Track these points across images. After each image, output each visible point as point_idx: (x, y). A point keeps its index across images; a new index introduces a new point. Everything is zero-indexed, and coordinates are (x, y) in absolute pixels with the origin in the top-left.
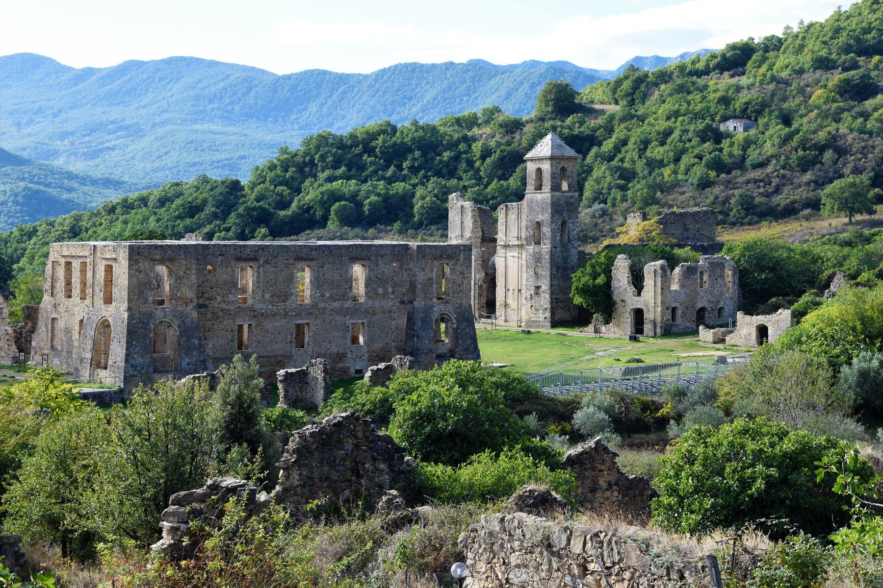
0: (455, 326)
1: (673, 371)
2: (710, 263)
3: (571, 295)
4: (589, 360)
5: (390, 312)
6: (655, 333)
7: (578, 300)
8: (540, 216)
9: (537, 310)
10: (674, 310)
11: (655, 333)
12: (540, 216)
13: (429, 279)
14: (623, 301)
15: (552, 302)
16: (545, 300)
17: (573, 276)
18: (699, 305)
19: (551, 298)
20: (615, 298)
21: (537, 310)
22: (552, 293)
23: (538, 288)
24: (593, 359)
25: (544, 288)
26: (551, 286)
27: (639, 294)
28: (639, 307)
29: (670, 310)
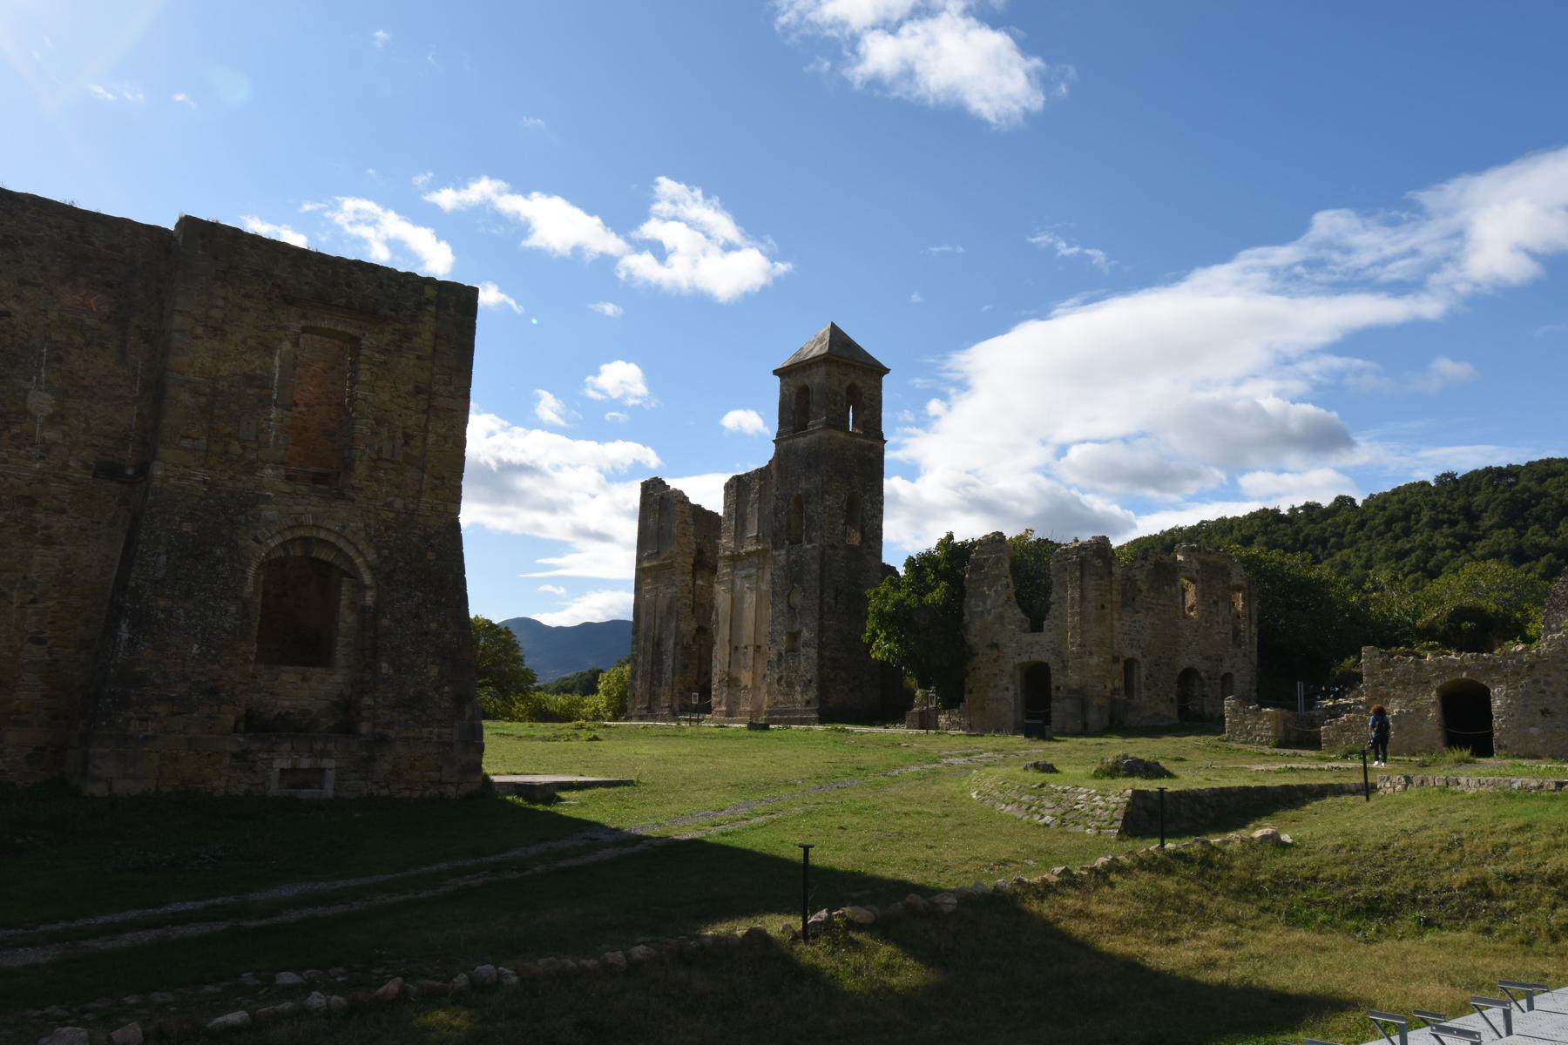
0: (369, 598)
1: (1425, 833)
2: (1201, 562)
3: (866, 637)
4: (922, 777)
5: (31, 501)
6: (1085, 725)
7: (882, 649)
8: (803, 484)
9: (790, 685)
10: (1129, 665)
11: (1085, 725)
12: (803, 484)
13: (250, 379)
14: (994, 646)
15: (821, 666)
16: (807, 663)
17: (870, 593)
18: (1184, 662)
19: (820, 656)
20: (973, 638)
21: (790, 685)
22: (821, 647)
23: (794, 636)
24: (935, 773)
25: (806, 634)
26: (822, 630)
27: (1037, 627)
28: (1036, 658)
29: (1120, 666)
